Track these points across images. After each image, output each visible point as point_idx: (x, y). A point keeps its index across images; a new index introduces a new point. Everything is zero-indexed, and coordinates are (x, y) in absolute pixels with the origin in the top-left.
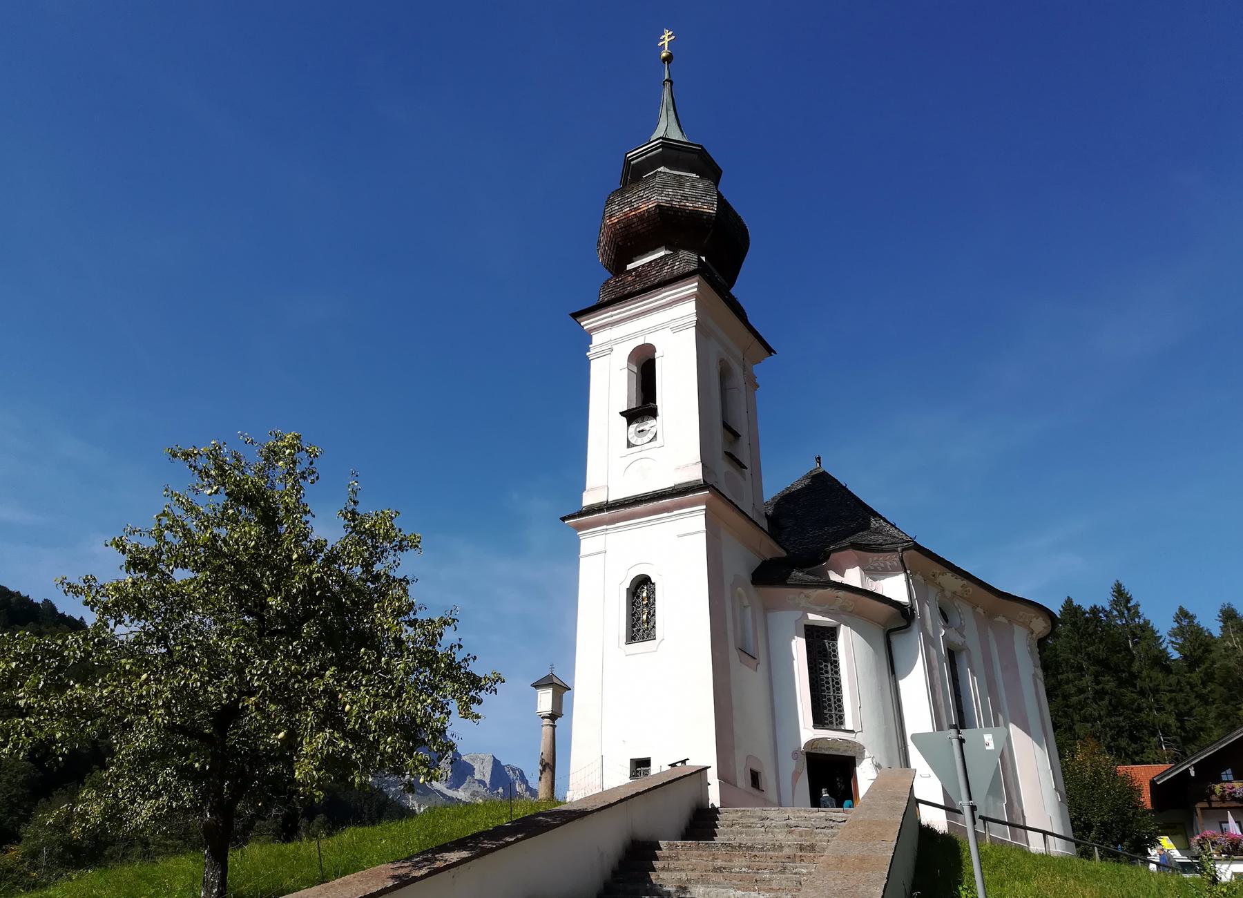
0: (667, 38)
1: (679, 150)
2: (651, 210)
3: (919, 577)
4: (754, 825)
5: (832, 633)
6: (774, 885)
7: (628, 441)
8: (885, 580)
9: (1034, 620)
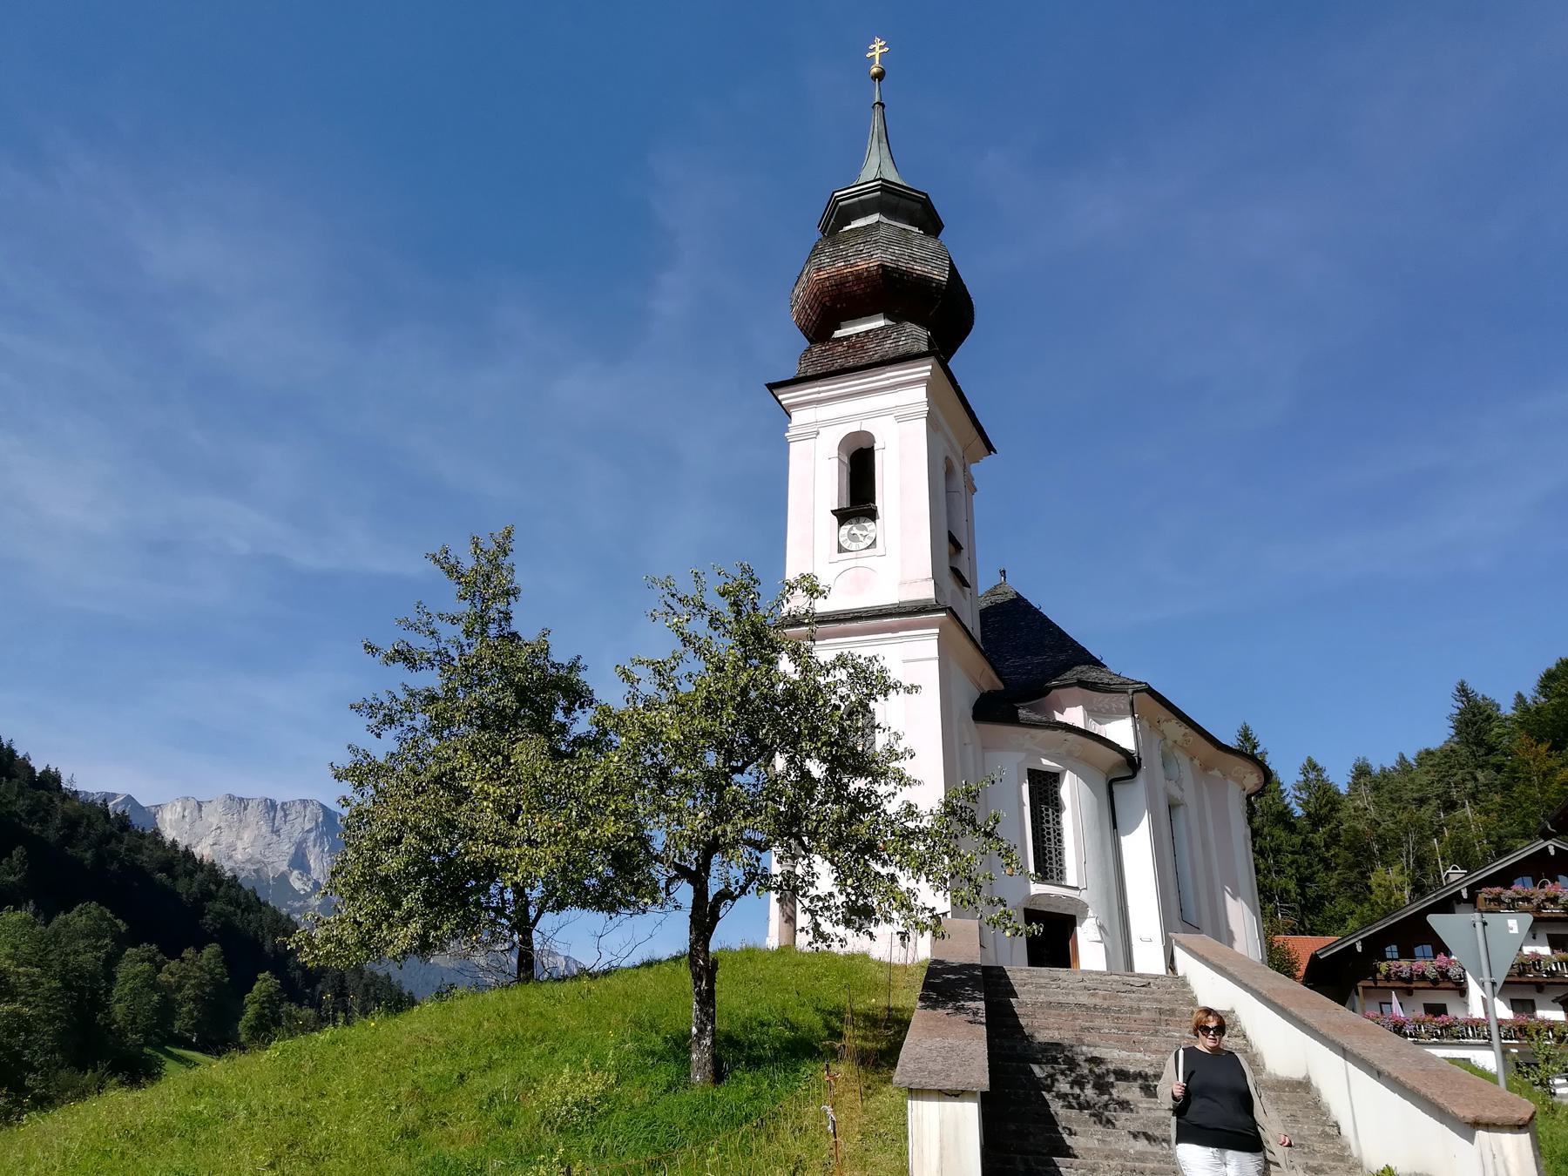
0: (877, 49)
1: (900, 196)
2: (872, 269)
3: (1145, 723)
4: (1049, 986)
5: (1054, 778)
6: (1153, 1046)
8: (1112, 723)
9: (1248, 776)
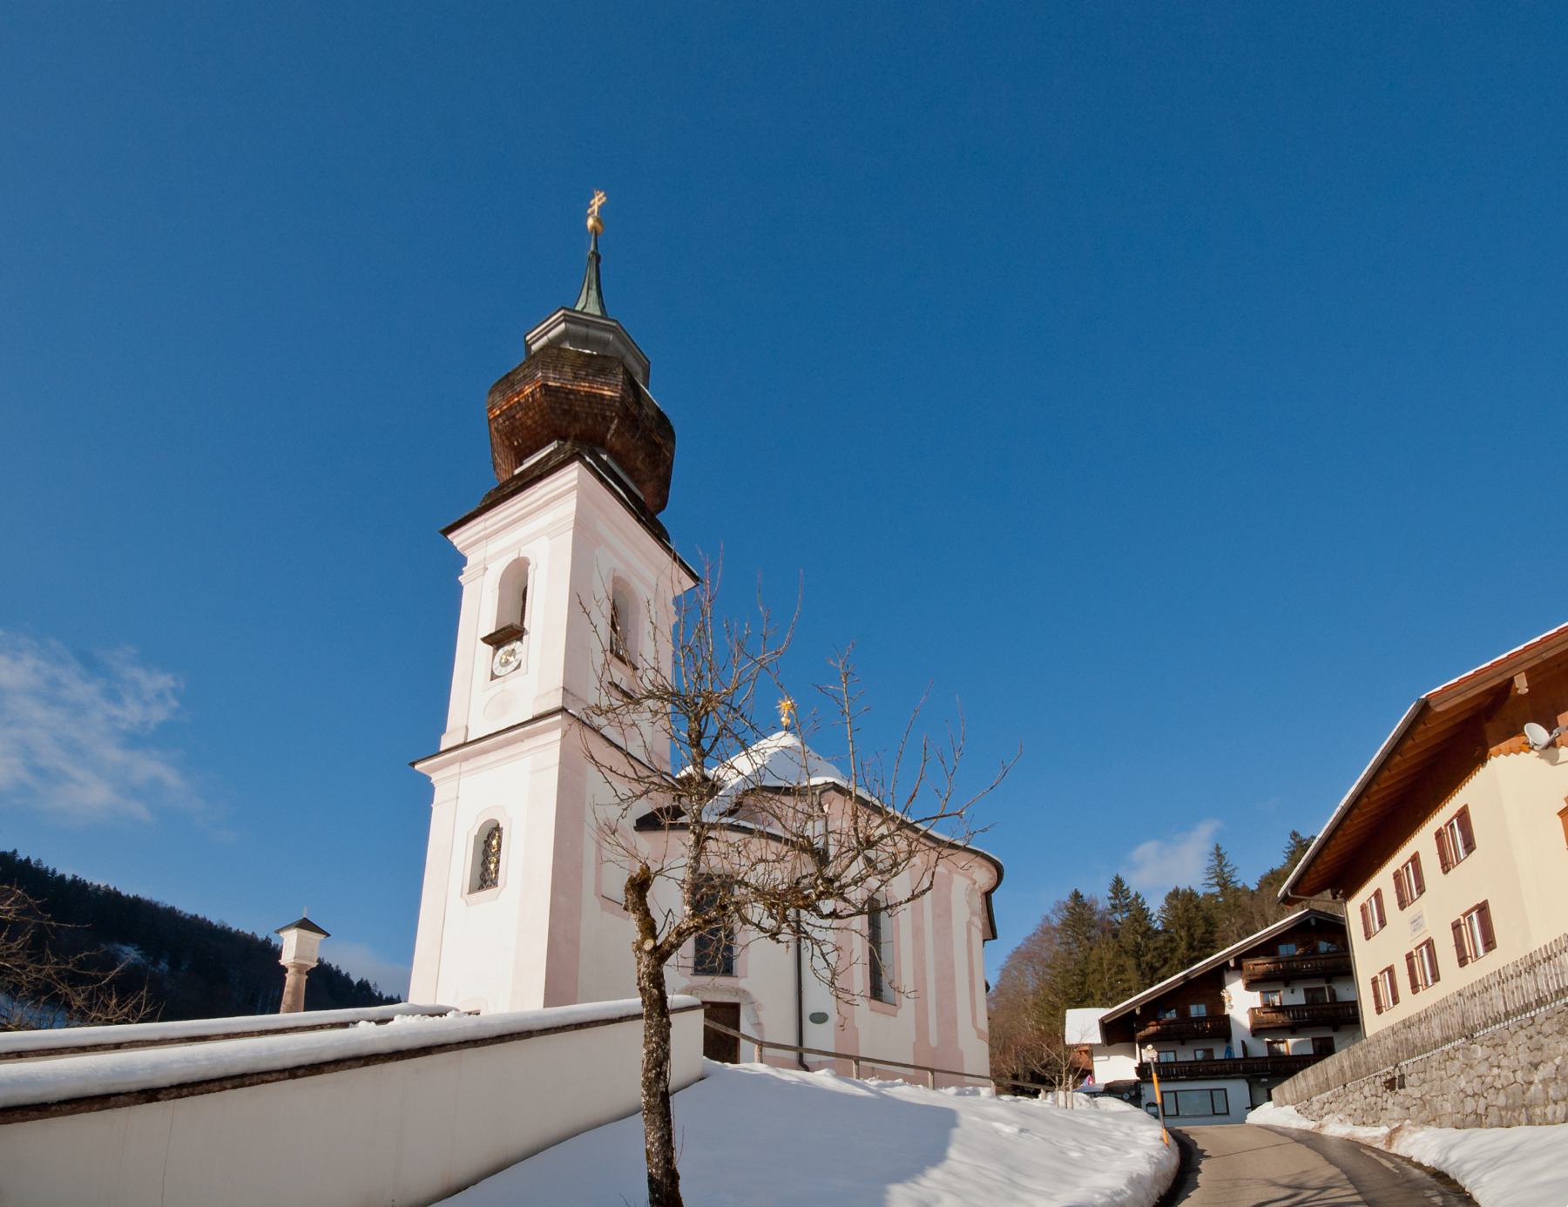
0: (598, 200)
7: (492, 672)
